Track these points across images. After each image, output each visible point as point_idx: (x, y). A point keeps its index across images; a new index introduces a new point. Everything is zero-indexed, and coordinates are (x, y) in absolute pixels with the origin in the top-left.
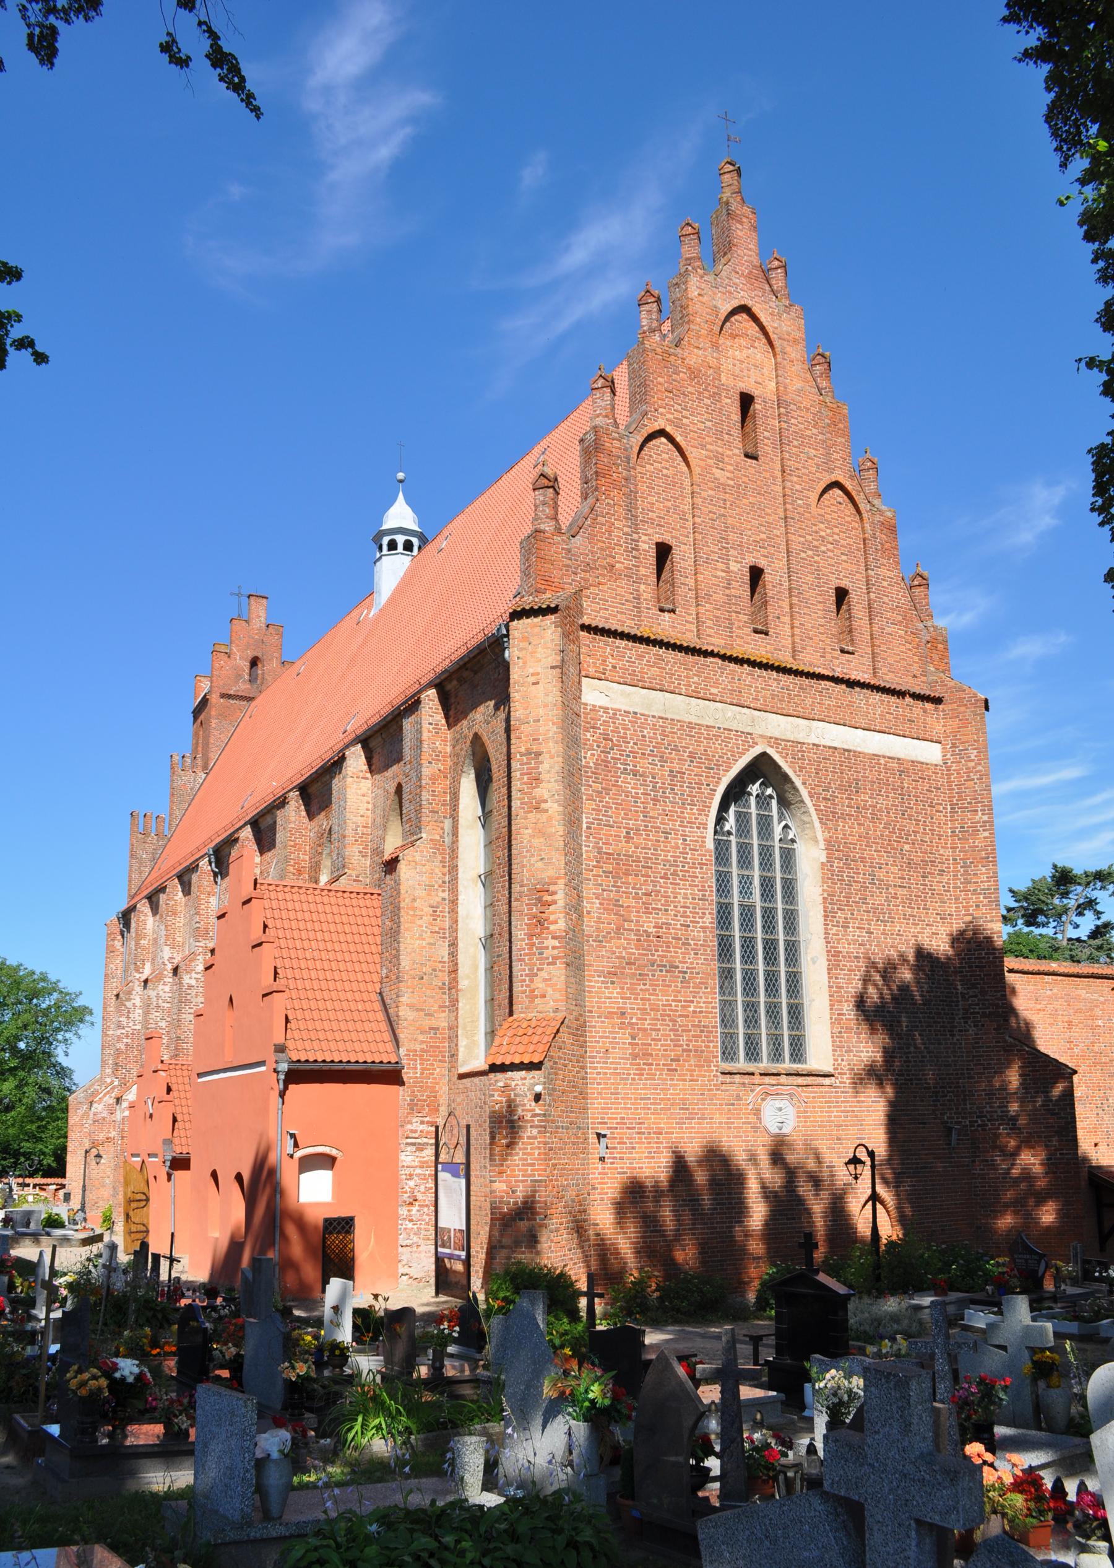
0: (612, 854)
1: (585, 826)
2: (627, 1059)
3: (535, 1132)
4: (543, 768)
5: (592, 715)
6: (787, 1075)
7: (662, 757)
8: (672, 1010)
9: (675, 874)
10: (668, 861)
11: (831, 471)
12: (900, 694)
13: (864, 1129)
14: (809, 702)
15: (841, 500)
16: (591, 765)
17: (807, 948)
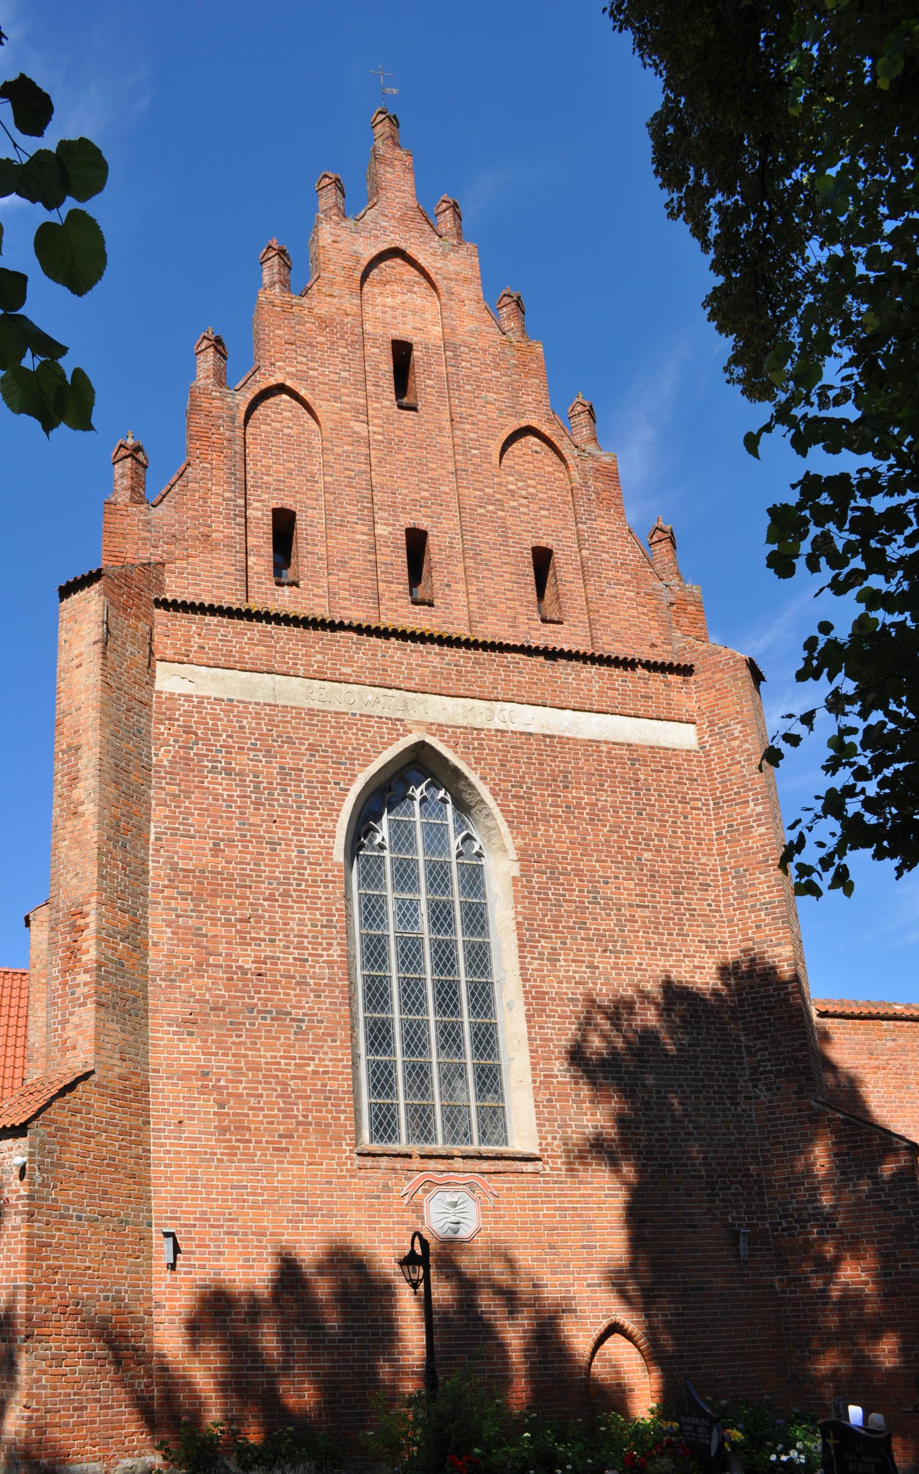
0: (193, 871)
1: (152, 837)
2: (212, 1134)
3: (18, 1219)
5: (169, 704)
6: (463, 1157)
7: (268, 751)
8: (280, 1070)
9: (286, 894)
10: (275, 878)
11: (519, 415)
12: (629, 664)
13: (595, 1234)
14: (488, 679)
15: (538, 449)
16: (166, 763)
17: (501, 991)
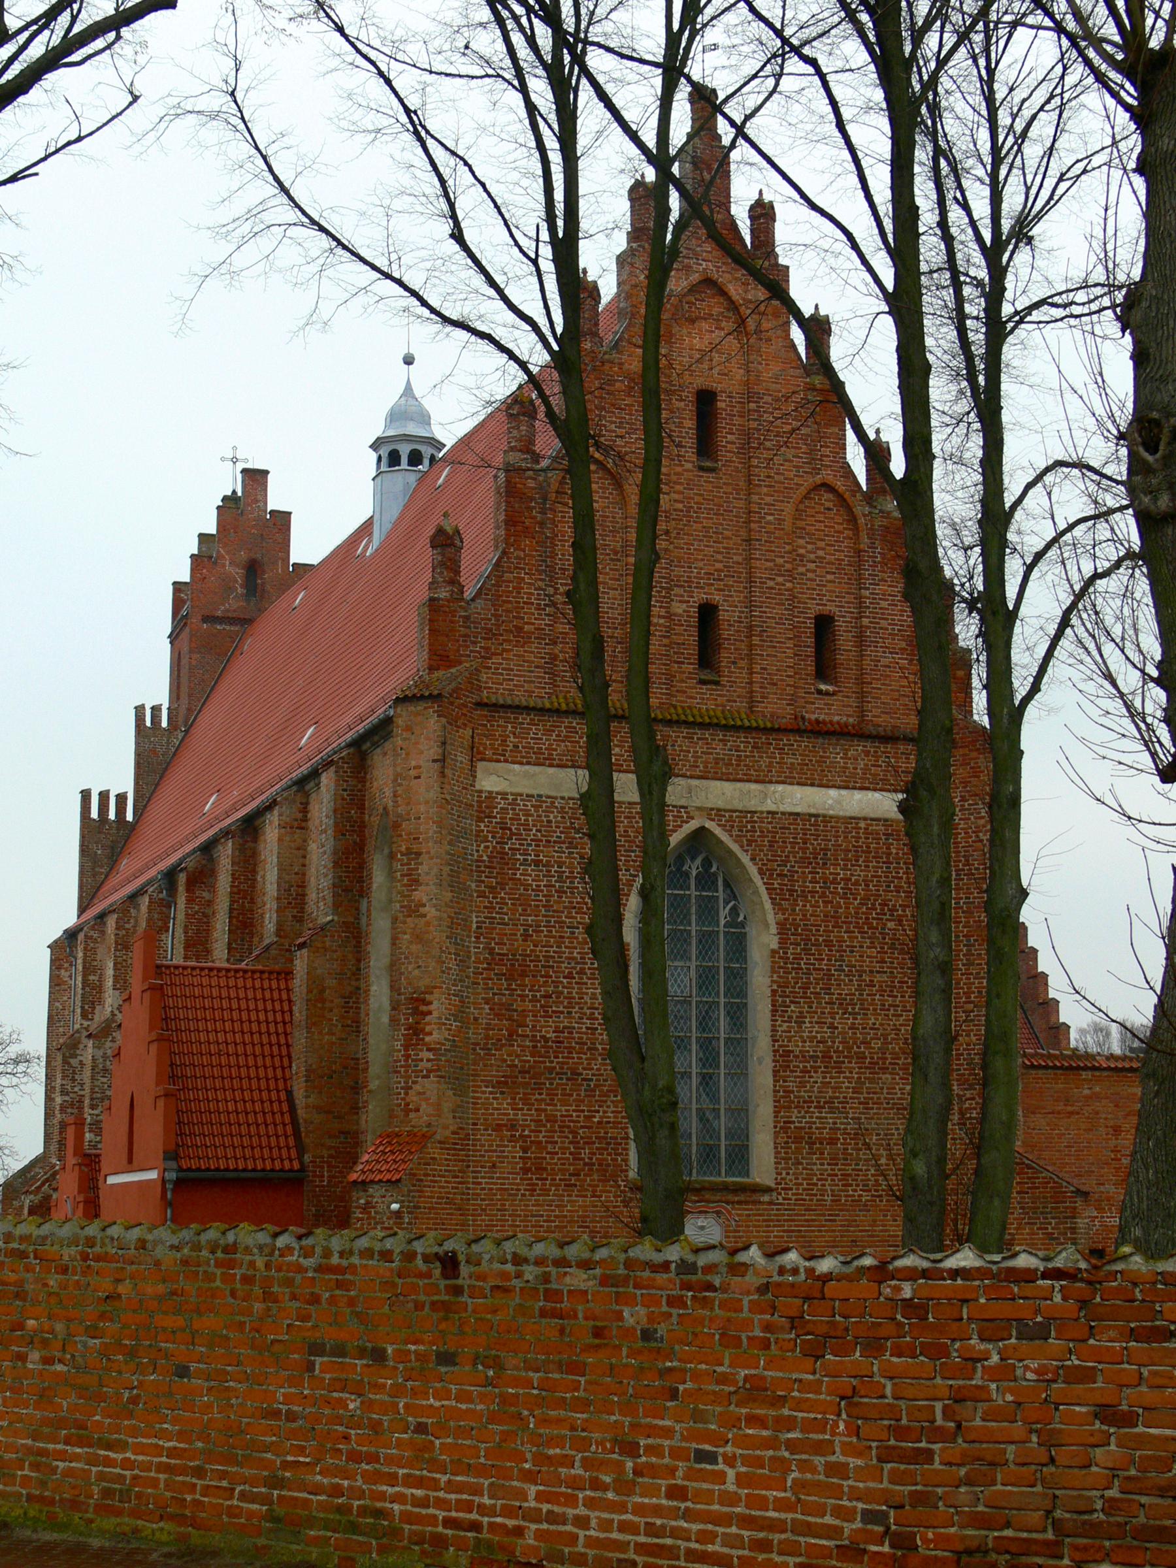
2: (518, 1174)
4: (423, 869)
9: (582, 972)
16: (485, 858)
17: (753, 1046)
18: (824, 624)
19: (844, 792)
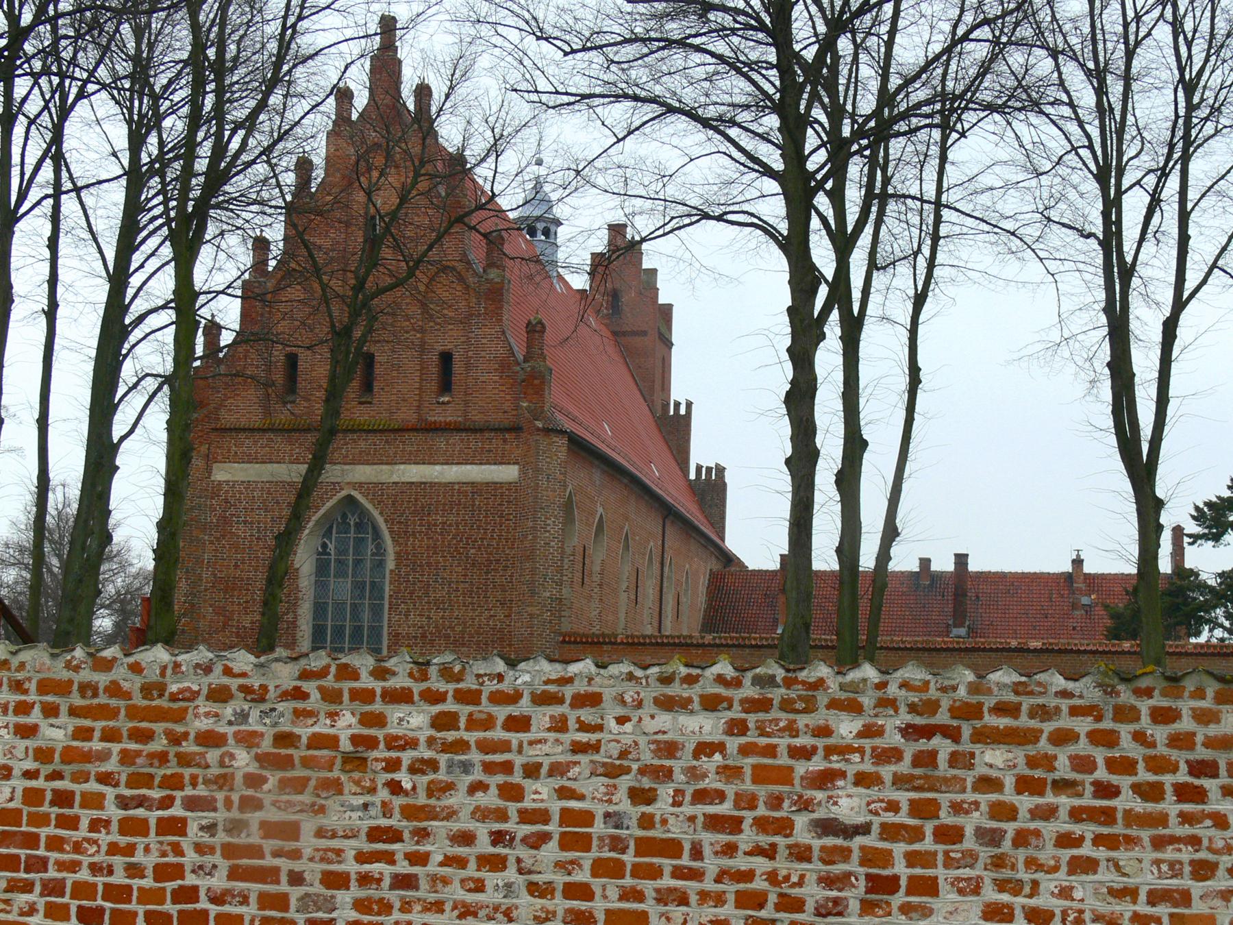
18: (446, 359)
19: (445, 467)
